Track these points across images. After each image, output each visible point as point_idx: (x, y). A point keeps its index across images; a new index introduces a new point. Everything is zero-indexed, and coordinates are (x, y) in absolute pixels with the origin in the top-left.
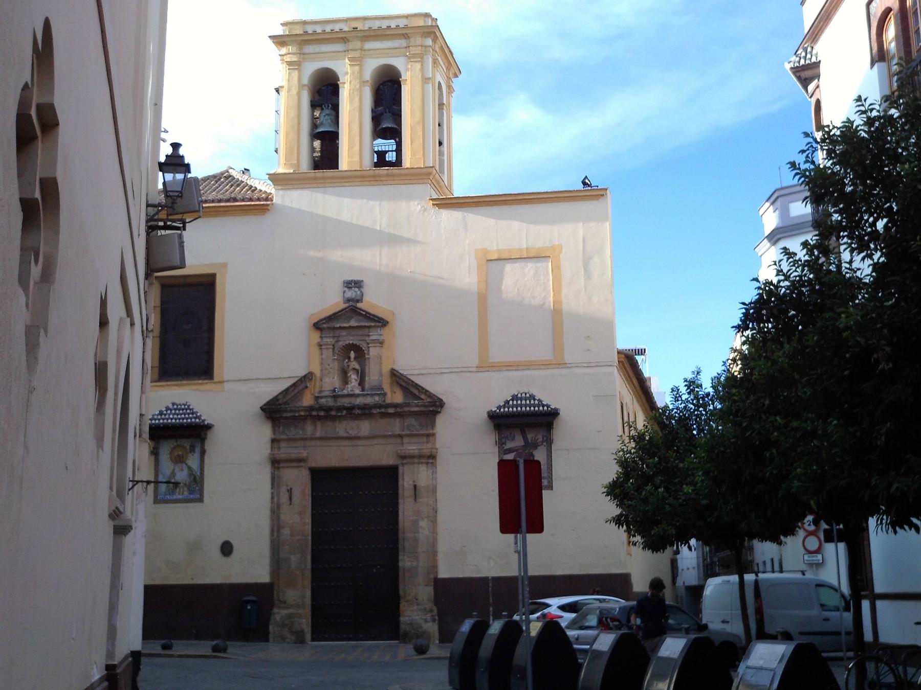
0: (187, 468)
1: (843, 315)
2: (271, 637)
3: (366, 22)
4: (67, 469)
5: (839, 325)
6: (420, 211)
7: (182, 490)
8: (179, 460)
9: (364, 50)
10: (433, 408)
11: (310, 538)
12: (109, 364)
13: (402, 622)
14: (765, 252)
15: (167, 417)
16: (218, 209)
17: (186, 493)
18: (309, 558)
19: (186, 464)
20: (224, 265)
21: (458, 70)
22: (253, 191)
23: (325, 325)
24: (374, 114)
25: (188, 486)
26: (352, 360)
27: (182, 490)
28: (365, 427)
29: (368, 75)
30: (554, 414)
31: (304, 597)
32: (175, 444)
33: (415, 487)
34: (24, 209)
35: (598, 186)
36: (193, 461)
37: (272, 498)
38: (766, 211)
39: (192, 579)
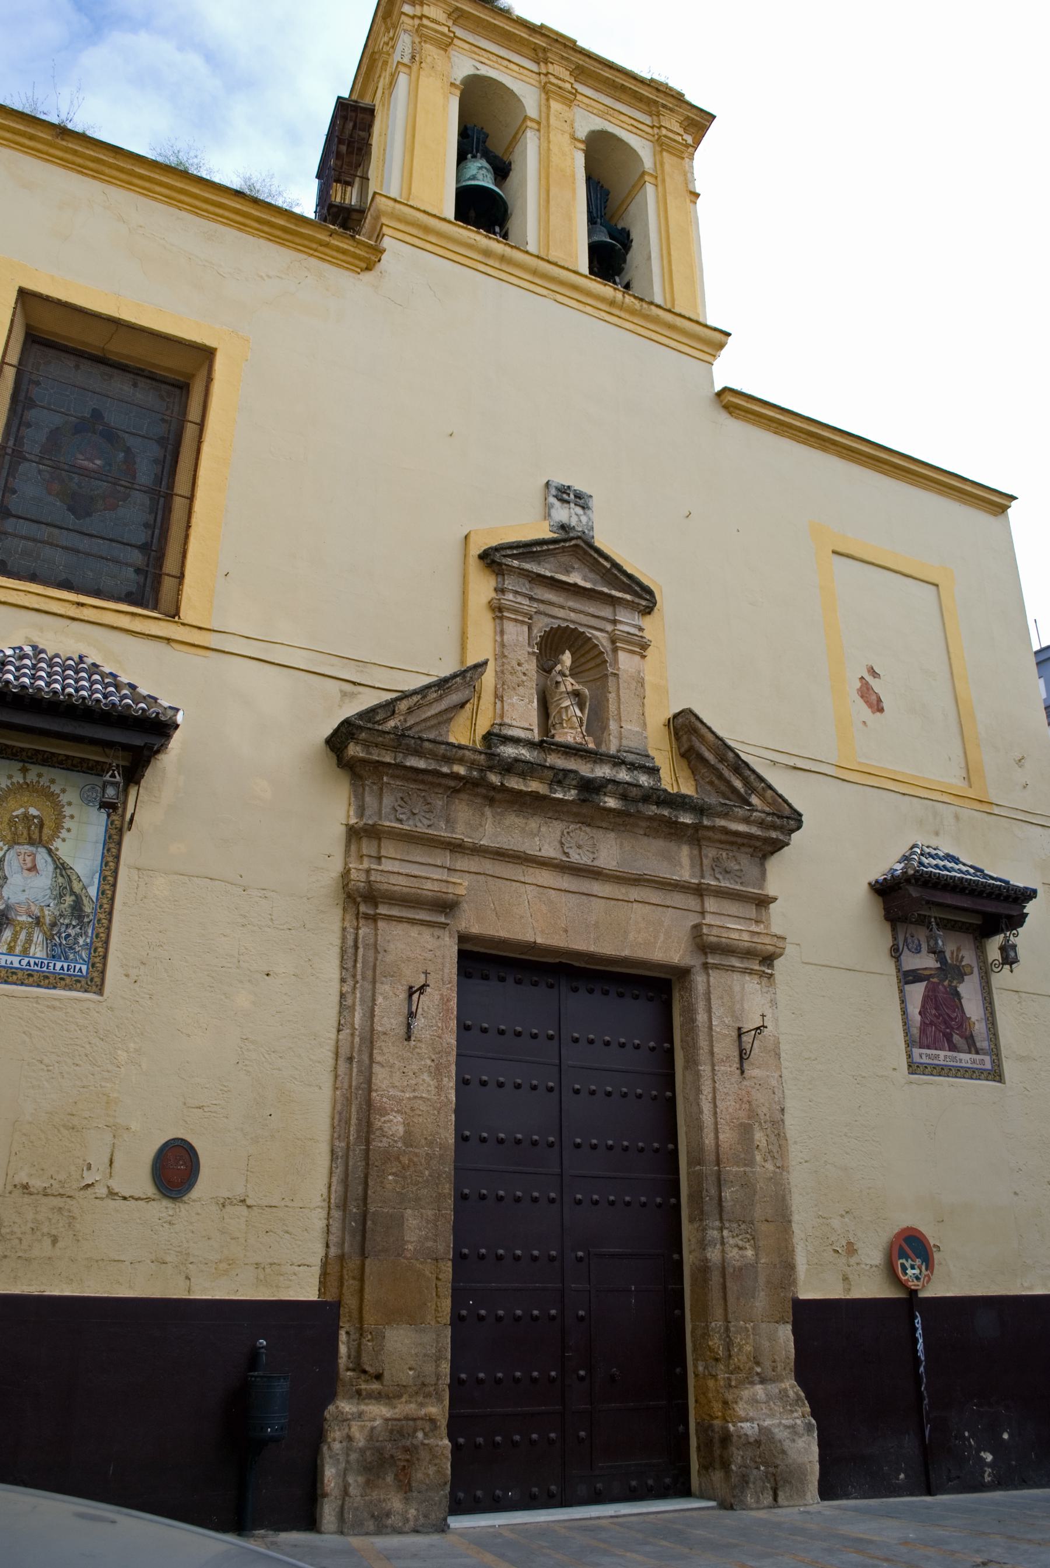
0: (51, 867)
2: (328, 1513)
3: (155, 450)
7: (23, 936)
10: (778, 833)
12: (328, 731)
14: (946, 638)
17: (38, 951)
19: (50, 852)
23: (516, 563)
25: (52, 930)
27: (23, 936)
32: (18, 778)
38: (946, 638)
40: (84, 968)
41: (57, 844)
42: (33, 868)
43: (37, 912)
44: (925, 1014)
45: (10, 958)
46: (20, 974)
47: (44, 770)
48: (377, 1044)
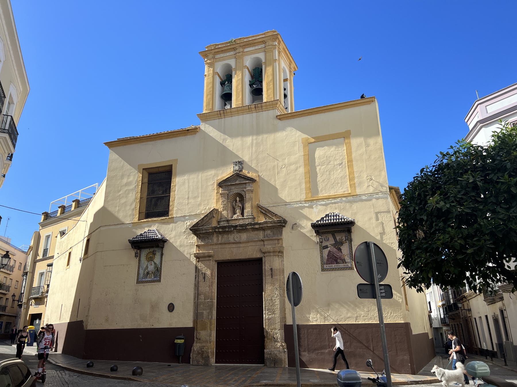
1: (348, 350)
4: (183, 274)
5: (471, 141)
6: (344, 160)
8: (150, 259)
9: (244, 52)
13: (258, 137)
17: (153, 277)
18: (214, 313)
19: (153, 261)
20: (176, 160)
24: (344, 340)
25: (154, 273)
28: (244, 236)
30: (352, 223)
31: (210, 336)
33: (271, 269)
34: (464, 362)
36: (157, 260)
37: (196, 278)
39: (153, 325)
41: (154, 260)
42: (152, 265)
45: (149, 279)
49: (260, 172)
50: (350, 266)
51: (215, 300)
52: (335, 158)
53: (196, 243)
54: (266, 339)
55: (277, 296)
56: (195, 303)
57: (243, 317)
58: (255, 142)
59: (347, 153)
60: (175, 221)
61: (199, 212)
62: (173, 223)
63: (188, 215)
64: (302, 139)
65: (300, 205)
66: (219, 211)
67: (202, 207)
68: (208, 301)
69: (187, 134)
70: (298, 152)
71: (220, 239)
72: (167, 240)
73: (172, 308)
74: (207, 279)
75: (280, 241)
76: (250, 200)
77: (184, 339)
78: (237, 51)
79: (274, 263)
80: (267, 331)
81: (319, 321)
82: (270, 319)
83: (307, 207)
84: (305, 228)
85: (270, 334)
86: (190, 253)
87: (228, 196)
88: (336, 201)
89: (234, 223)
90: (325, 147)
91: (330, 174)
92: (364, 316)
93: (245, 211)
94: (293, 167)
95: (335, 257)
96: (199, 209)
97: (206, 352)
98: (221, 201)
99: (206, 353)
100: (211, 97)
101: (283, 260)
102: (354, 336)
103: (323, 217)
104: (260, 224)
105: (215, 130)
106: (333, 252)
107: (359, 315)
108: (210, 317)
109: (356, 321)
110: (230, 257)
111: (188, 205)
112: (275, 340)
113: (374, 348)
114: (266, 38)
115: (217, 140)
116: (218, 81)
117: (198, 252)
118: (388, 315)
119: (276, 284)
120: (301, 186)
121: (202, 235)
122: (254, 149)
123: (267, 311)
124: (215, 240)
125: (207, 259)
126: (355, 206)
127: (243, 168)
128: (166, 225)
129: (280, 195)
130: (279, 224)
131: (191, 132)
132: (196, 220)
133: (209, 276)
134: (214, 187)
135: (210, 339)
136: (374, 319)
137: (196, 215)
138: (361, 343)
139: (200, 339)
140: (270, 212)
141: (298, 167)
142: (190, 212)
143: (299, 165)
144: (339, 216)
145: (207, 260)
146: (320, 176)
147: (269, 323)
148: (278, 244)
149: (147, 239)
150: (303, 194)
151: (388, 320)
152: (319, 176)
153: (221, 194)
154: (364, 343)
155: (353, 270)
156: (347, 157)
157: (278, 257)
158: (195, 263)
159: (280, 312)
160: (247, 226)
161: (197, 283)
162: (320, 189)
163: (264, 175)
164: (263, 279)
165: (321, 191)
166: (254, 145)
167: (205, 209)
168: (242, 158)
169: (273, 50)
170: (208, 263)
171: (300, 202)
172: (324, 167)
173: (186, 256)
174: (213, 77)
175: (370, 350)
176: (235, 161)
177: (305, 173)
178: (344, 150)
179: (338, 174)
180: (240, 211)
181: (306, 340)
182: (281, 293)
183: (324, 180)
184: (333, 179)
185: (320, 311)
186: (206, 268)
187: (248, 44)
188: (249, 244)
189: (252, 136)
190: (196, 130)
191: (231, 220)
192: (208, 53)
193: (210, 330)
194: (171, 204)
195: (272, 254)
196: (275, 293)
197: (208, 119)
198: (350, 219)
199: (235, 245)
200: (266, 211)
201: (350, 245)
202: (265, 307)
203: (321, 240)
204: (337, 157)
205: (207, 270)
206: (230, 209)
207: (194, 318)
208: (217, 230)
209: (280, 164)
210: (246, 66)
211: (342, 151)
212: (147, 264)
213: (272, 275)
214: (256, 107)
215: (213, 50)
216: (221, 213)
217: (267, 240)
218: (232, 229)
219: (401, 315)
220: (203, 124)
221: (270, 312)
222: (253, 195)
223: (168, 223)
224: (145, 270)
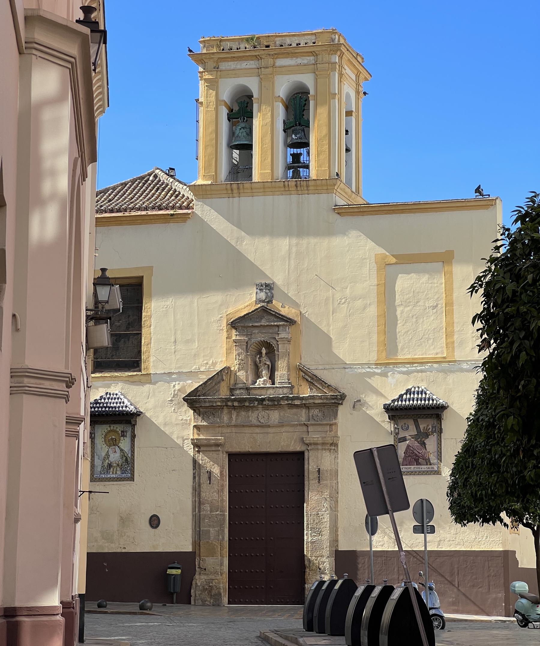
6: (440, 300)
11: (227, 514)
13: (300, 242)
15: (101, 405)
16: (119, 219)
17: (119, 472)
19: (118, 447)
20: (150, 269)
21: (369, 75)
22: (177, 196)
26: (263, 356)
28: (275, 416)
29: (226, 95)
30: (443, 408)
31: (222, 564)
33: (319, 471)
35: (489, 195)
36: (125, 444)
37: (194, 478)
39: (124, 548)
40: (130, 475)
41: (120, 444)
42: (115, 452)
43: (117, 463)
44: (407, 453)
45: (113, 475)
46: (115, 478)
47: (114, 425)
48: (201, 486)
49: (303, 308)
50: (437, 469)
51: (227, 513)
52: (426, 295)
53: (193, 421)
54: (308, 570)
55: (327, 509)
56: (194, 516)
57: (272, 538)
58: (294, 249)
59: (445, 290)
60: (152, 382)
61: (195, 369)
62: (150, 383)
63: (177, 371)
64: (375, 255)
65: (368, 370)
66: (231, 371)
67: (200, 360)
68: (217, 513)
69: (169, 220)
70: (368, 278)
71: (234, 417)
72: (142, 413)
73: (156, 522)
74: (213, 480)
75: (334, 427)
76: (286, 356)
77: (181, 568)
78: (263, 63)
79: (323, 461)
80: (309, 559)
81: (386, 545)
82: (315, 542)
83: (378, 374)
84: (373, 409)
85: (313, 564)
86: (183, 438)
87: (247, 346)
88: (424, 367)
89: (259, 394)
90: (412, 274)
91: (417, 322)
92: (449, 541)
93: (277, 374)
94: (359, 303)
95: (416, 455)
96: (195, 363)
97: (216, 587)
98: (235, 353)
99: (215, 589)
100: (214, 152)
101: (338, 456)
102: (433, 567)
103: (403, 393)
104: (303, 399)
105: (222, 217)
106: (414, 448)
107: (442, 539)
108: (221, 537)
109: (438, 547)
110: (251, 447)
111: (176, 353)
112: (321, 571)
113: (459, 584)
114: (318, 47)
115: (225, 238)
116: (224, 112)
117: (196, 437)
118: (482, 539)
119: (324, 493)
120: (371, 338)
121: (204, 410)
122: (292, 262)
123: (311, 530)
124: (225, 418)
125: (213, 448)
126: (451, 378)
127: (273, 296)
128: (138, 387)
129: (335, 351)
130: (333, 401)
131: (178, 218)
132: (191, 381)
133: (217, 475)
134: (221, 326)
135: (221, 570)
136: (463, 545)
137: (191, 374)
138: (443, 576)
139: (205, 569)
140: (319, 380)
141: (367, 304)
142: (179, 368)
143: (369, 302)
144: (426, 394)
145: (213, 451)
146: (402, 324)
147: (313, 548)
148: (330, 431)
149: (111, 411)
150: (373, 351)
151: (482, 546)
152: (400, 323)
153: (235, 341)
154: (446, 577)
155: (440, 475)
156: (446, 297)
157: (330, 451)
158: (192, 454)
159: (330, 533)
160: (281, 401)
161: (197, 485)
162: (400, 346)
163: (310, 313)
164: (306, 484)
165: (402, 349)
166: (293, 256)
167: (207, 363)
168: (271, 278)
169: (330, 74)
170: (214, 455)
171: (369, 365)
172: (408, 308)
173: (176, 441)
174: (216, 109)
175: (454, 585)
176: (258, 282)
177: (377, 315)
178: (442, 284)
179: (430, 324)
180: (268, 373)
181: (367, 572)
182: (333, 506)
183: (408, 331)
184: (422, 330)
185: (388, 533)
186: (211, 463)
187: (283, 54)
188: (283, 429)
189: (289, 238)
190: (188, 216)
191: (253, 388)
192: (206, 59)
193: (220, 556)
194: (144, 349)
195: (320, 447)
196: (322, 505)
197: (209, 196)
198: (441, 401)
199: (259, 428)
200: (313, 379)
201: (439, 437)
202: (308, 524)
203: (397, 431)
204: (430, 295)
205: (213, 467)
206: (251, 368)
207: (194, 538)
208: (230, 404)
209: (338, 296)
210: (279, 96)
211: (438, 284)
212: (108, 451)
213: (319, 480)
214: (299, 185)
215: (216, 54)
216: (236, 374)
217: (312, 425)
218: (256, 403)
219: (500, 540)
220: (200, 203)
221: (315, 533)
222: (290, 348)
223: (141, 383)
224: (104, 459)
